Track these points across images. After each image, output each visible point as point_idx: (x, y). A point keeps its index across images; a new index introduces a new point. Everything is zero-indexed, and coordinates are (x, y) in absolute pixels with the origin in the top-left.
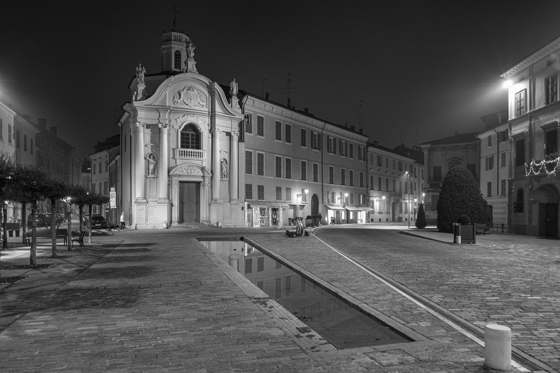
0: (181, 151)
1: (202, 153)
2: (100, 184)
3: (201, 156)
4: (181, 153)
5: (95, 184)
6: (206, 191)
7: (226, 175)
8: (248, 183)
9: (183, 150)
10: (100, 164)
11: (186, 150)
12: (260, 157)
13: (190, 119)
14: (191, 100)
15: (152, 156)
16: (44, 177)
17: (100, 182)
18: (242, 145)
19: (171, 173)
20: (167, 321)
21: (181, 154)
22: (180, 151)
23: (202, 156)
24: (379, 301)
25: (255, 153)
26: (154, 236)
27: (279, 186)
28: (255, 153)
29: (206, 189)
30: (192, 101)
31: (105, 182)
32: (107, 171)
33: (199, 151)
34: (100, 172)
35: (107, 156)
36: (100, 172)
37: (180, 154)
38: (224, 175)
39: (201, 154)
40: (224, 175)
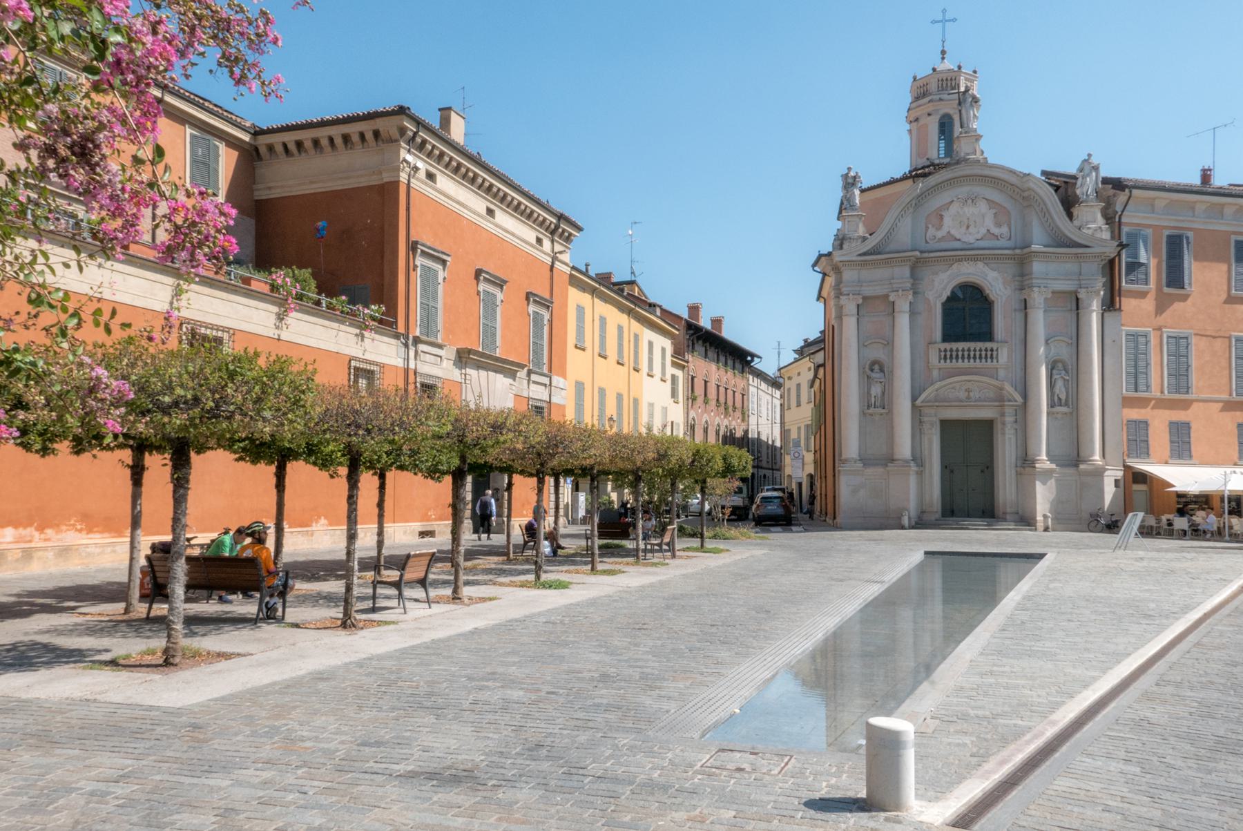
1: (940, 359)
2: (799, 428)
4: (943, 354)
5: (789, 430)
6: (1007, 441)
9: (948, 346)
10: (799, 386)
11: (955, 345)
13: (970, 272)
14: (968, 227)
15: (876, 367)
16: (379, 461)
19: (918, 402)
20: (656, 748)
22: (940, 351)
23: (997, 358)
24: (268, 732)
26: (479, 577)
29: (1007, 436)
30: (971, 230)
32: (809, 402)
33: (989, 345)
34: (799, 405)
35: (810, 369)
36: (799, 405)
37: (940, 355)
39: (995, 353)
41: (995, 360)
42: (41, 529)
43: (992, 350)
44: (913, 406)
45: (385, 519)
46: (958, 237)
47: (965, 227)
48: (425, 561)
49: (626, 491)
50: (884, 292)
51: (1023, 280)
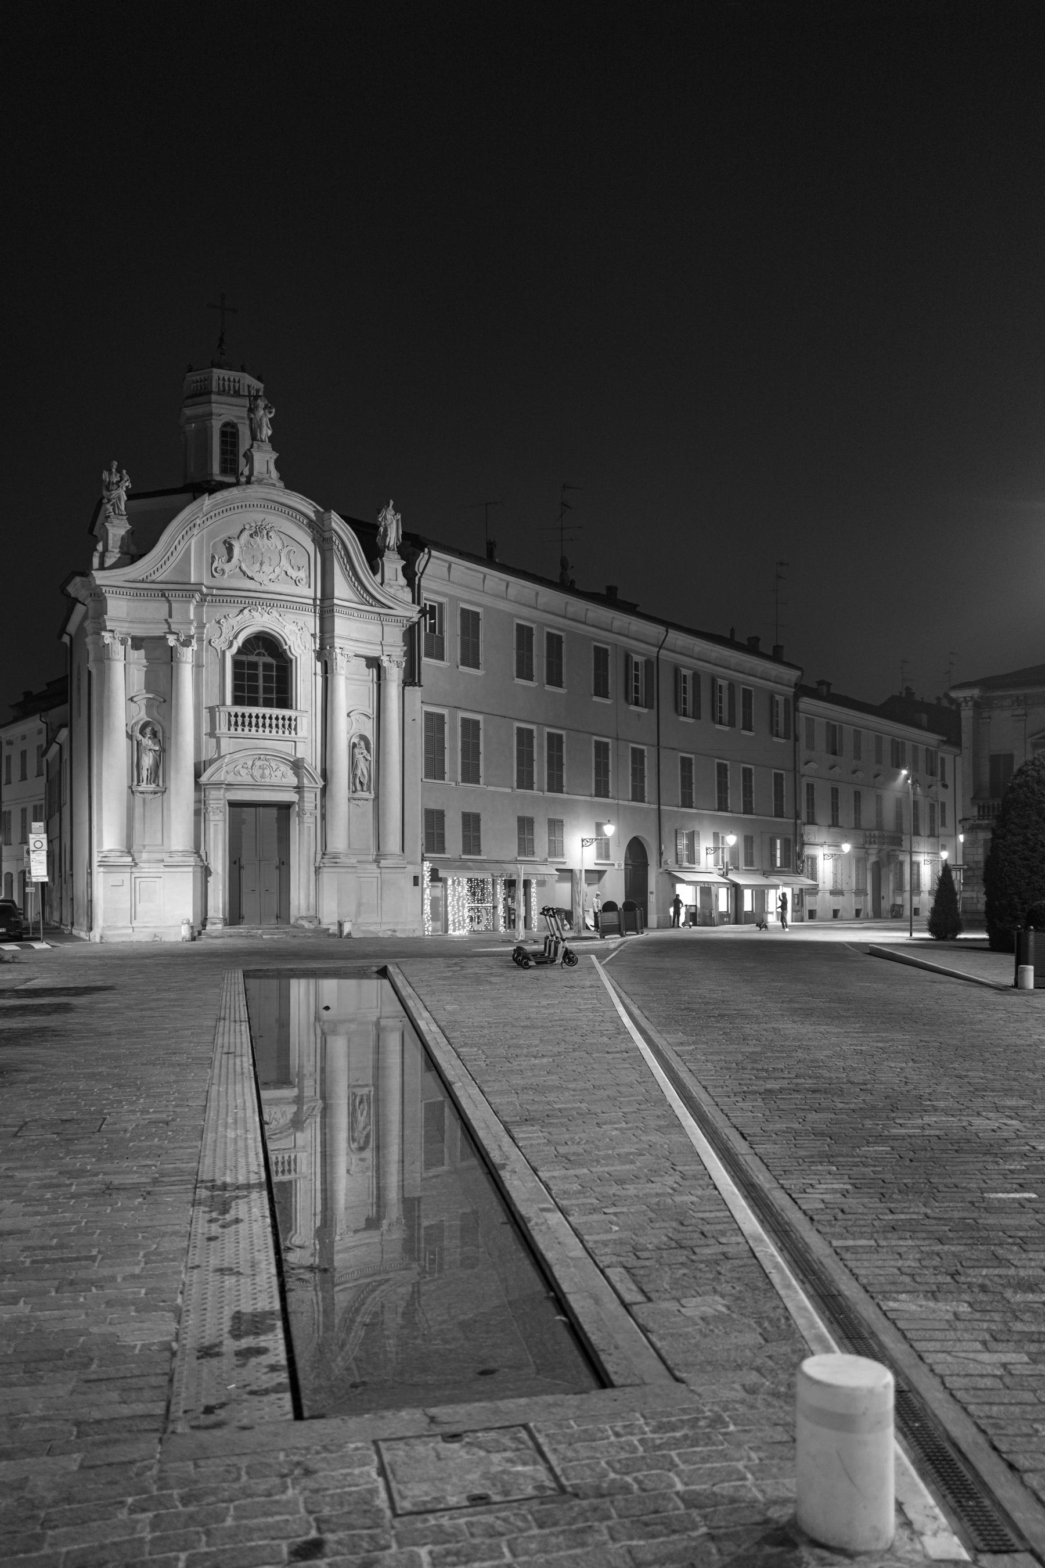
0: (233, 714)
3: (293, 727)
5: (10, 813)
6: (306, 831)
7: (365, 782)
8: (432, 806)
9: (240, 710)
10: (24, 754)
11: (248, 710)
12: (470, 729)
13: (260, 621)
14: (261, 564)
15: (148, 730)
17: (23, 806)
18: (414, 693)
19: (204, 779)
21: (233, 723)
23: (295, 729)
25: (453, 718)
27: (528, 814)
28: (453, 718)
31: (35, 807)
33: (286, 713)
34: (24, 777)
36: (24, 777)
37: (229, 721)
38: (361, 783)
40: (361, 783)
41: (293, 732)
42: (956, 894)
43: (290, 719)
44: (197, 783)
45: (817, 810)
47: (258, 565)
48: (1028, 1547)
49: (904, 772)
50: (159, 633)
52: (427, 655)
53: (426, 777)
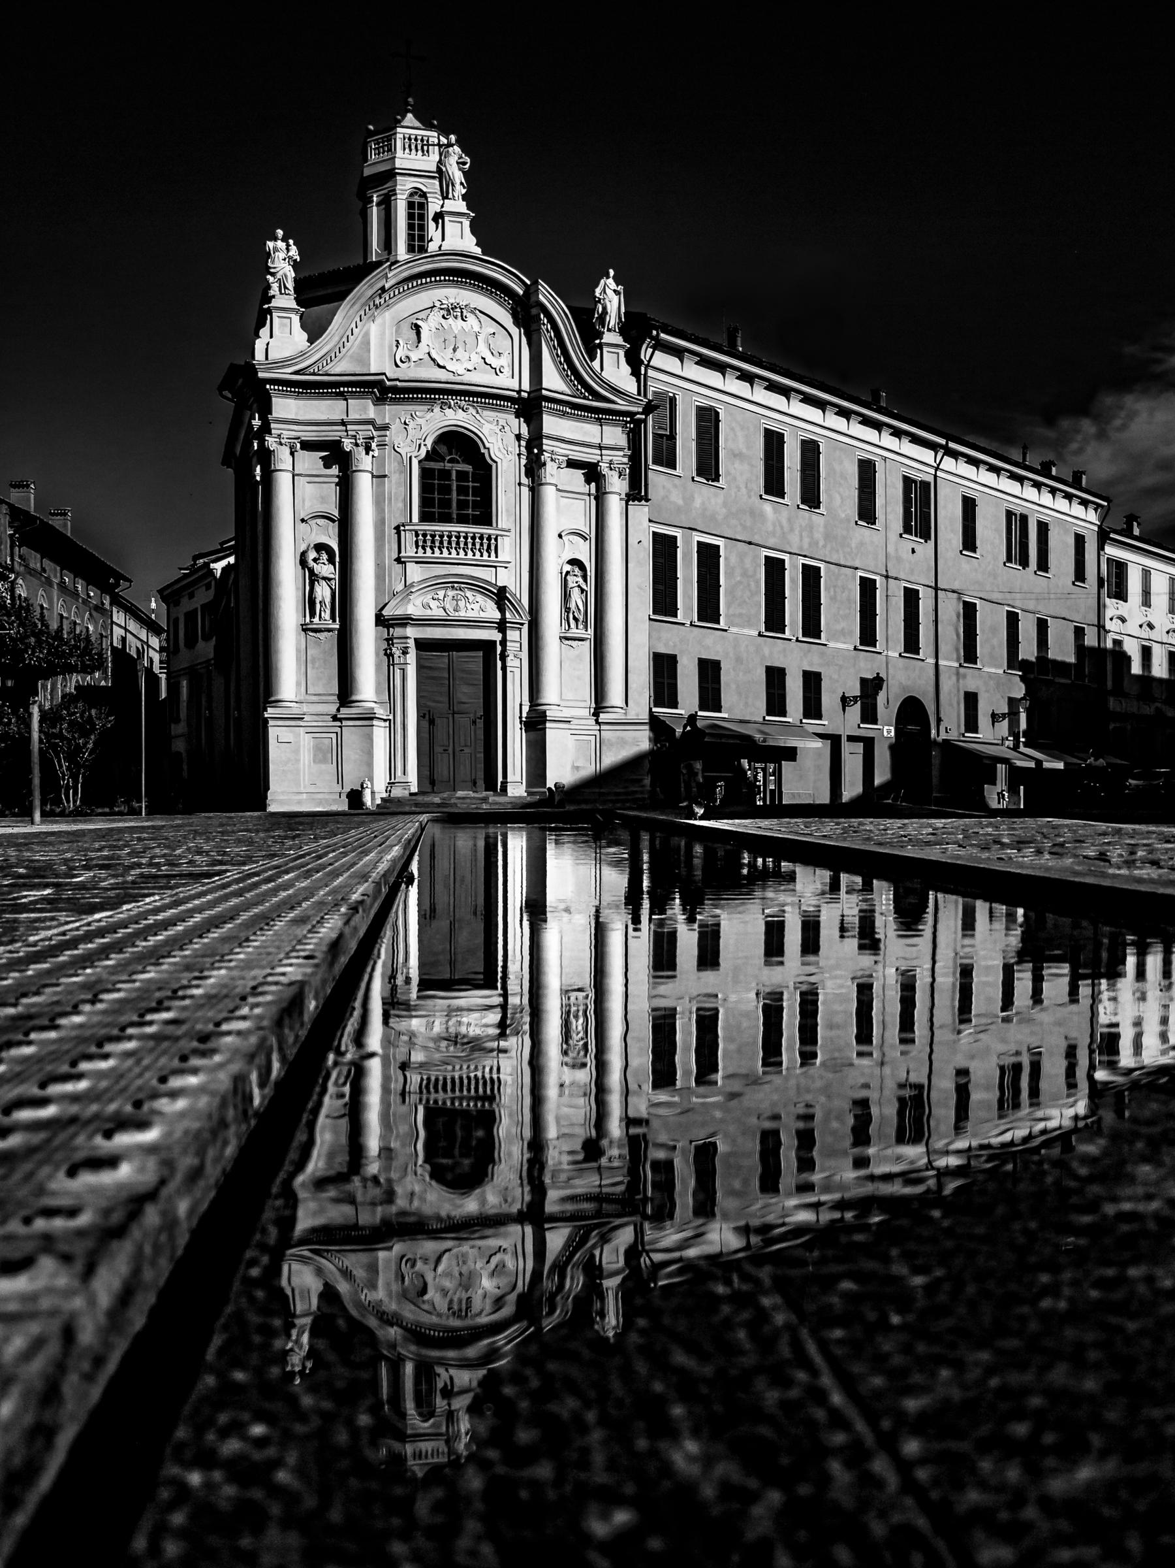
8: (662, 650)
18: (639, 512)
28: (687, 542)
33: (486, 531)
37: (417, 542)
46: (441, 364)
51: (534, 443)
52: (654, 463)
53: (654, 613)
